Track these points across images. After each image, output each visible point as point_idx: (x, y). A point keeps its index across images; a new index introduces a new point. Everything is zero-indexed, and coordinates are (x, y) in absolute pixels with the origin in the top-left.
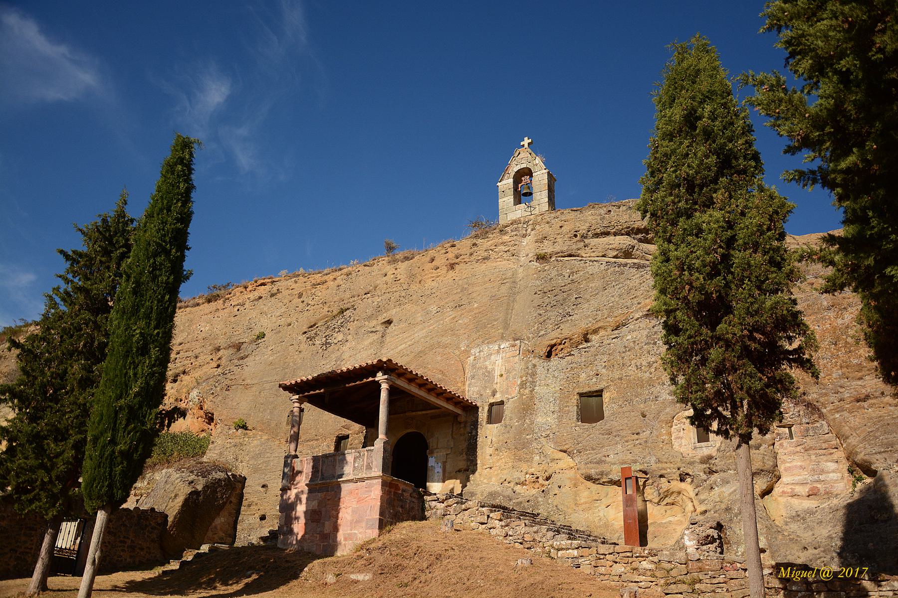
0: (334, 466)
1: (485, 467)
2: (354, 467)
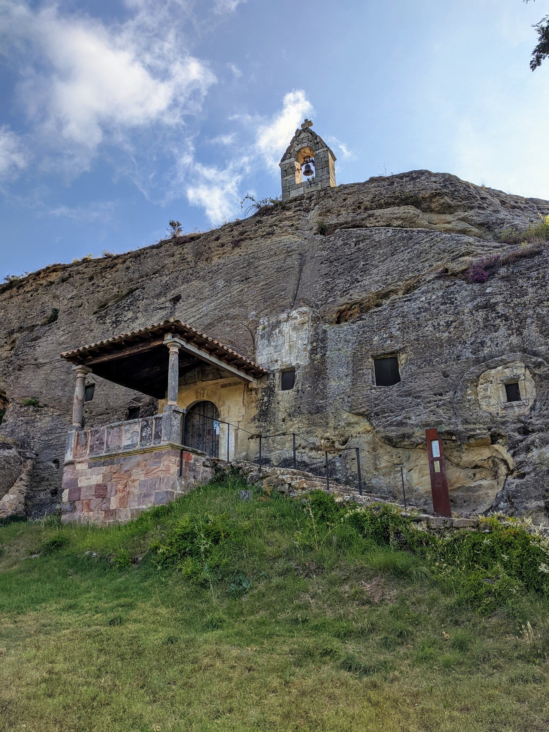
0: (120, 437)
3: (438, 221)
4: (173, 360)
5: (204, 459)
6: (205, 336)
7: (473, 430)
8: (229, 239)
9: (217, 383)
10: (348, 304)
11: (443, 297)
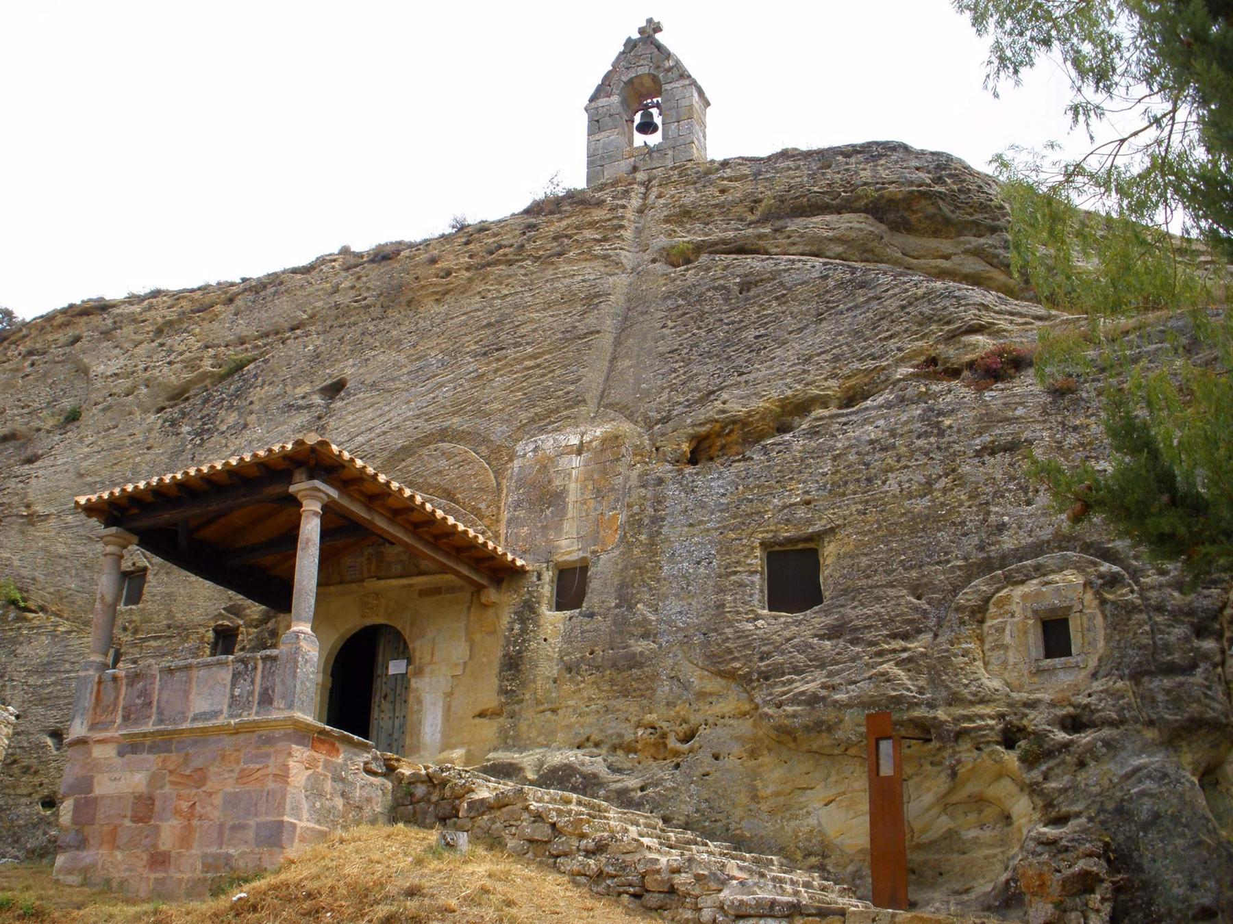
0: (187, 693)
1: (541, 708)
2: (232, 696)
3: (922, 253)
4: (311, 529)
5: (367, 757)
6: (382, 478)
7: (969, 719)
8: (462, 260)
9: (410, 586)
10: (717, 421)
11: (922, 418)
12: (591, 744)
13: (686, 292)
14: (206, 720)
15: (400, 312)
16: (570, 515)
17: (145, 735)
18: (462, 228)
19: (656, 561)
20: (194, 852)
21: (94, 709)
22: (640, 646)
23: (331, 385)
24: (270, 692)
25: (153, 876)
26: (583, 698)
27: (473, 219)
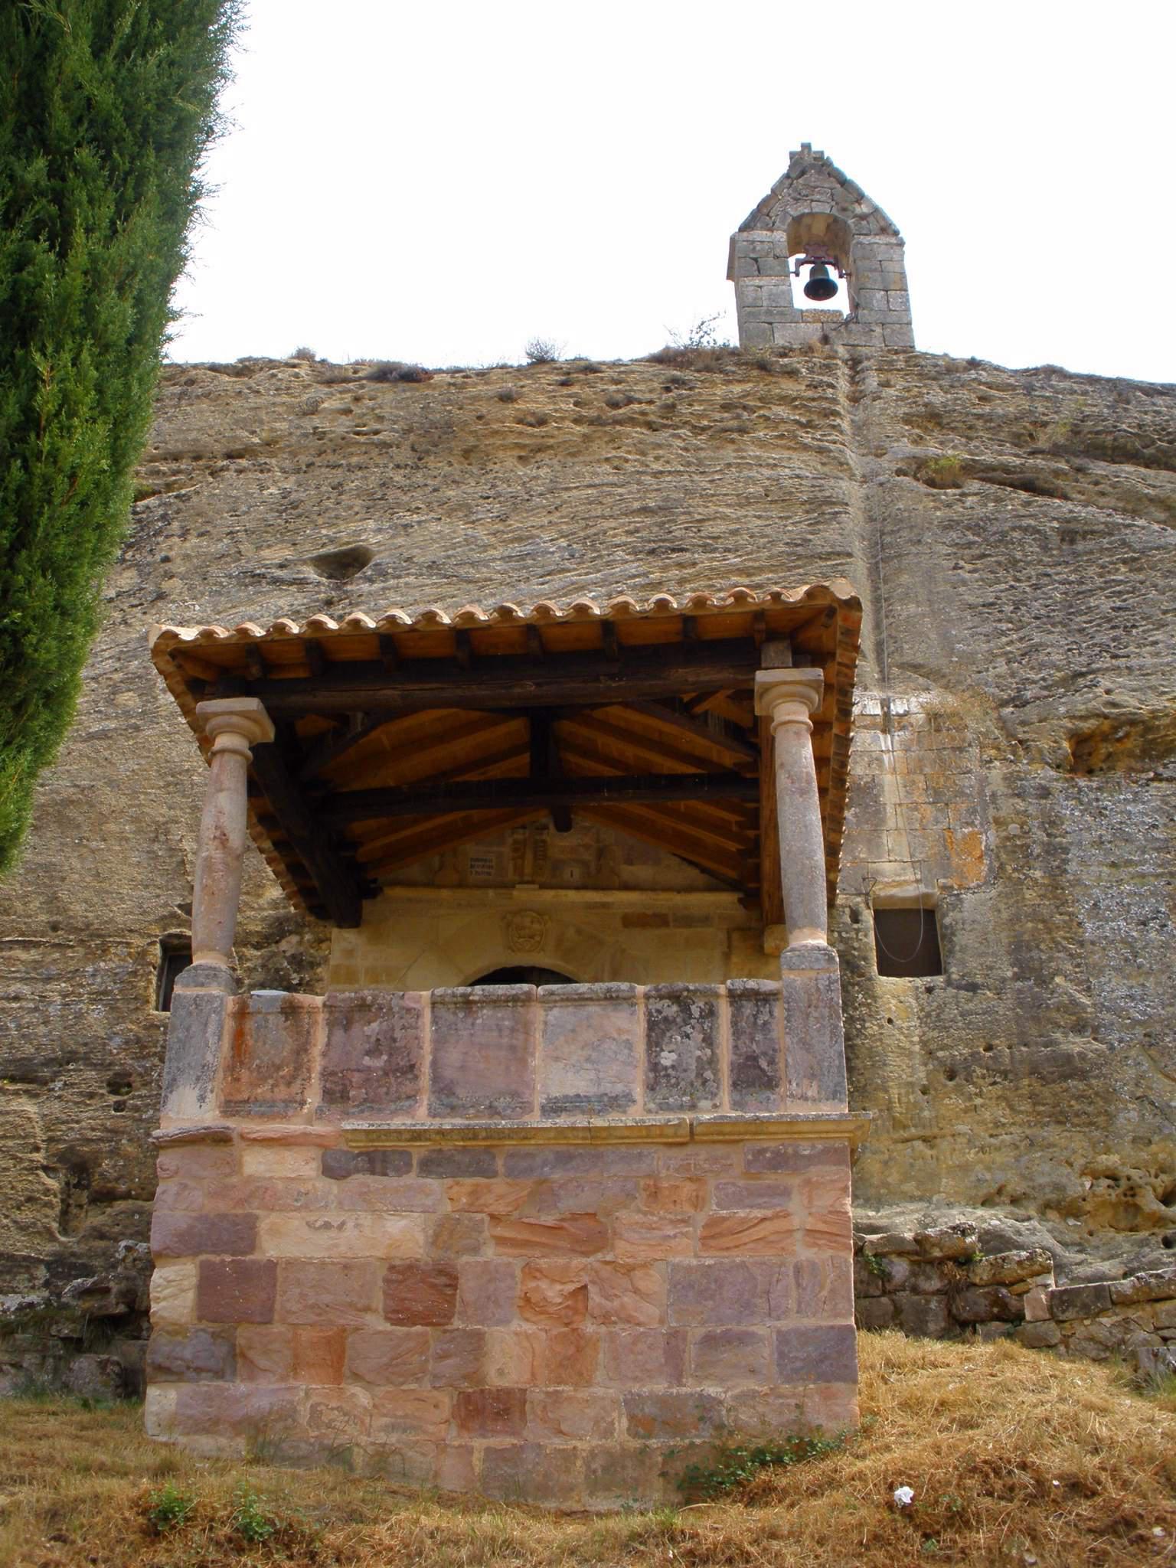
0: (519, 1055)
2: (655, 1067)
9: (605, 905)
10: (1106, 717)
12: (1005, 1199)
13: (977, 525)
14: (592, 1112)
15: (450, 464)
16: (891, 823)
17: (417, 1135)
18: (541, 361)
19: (1070, 914)
20: (599, 1391)
21: (231, 1069)
22: (1075, 1044)
23: (336, 555)
24: (763, 1064)
25: (479, 1443)
26: (983, 1122)
27: (565, 352)
